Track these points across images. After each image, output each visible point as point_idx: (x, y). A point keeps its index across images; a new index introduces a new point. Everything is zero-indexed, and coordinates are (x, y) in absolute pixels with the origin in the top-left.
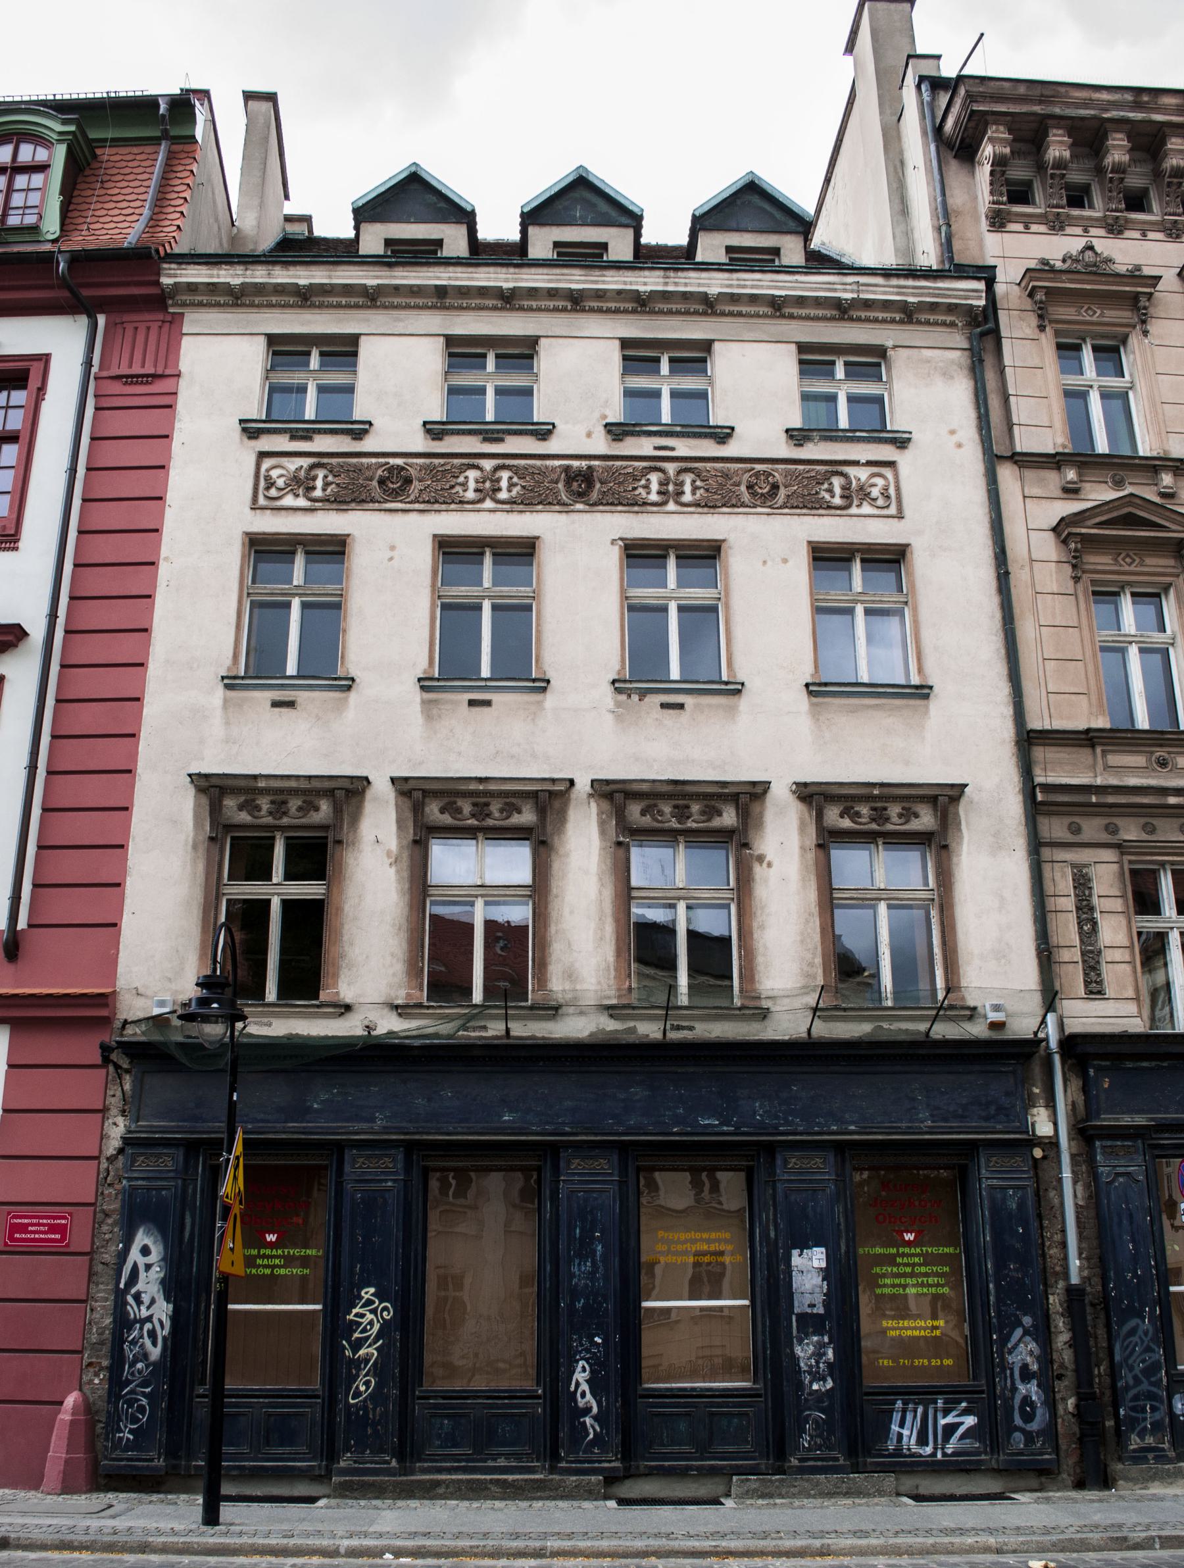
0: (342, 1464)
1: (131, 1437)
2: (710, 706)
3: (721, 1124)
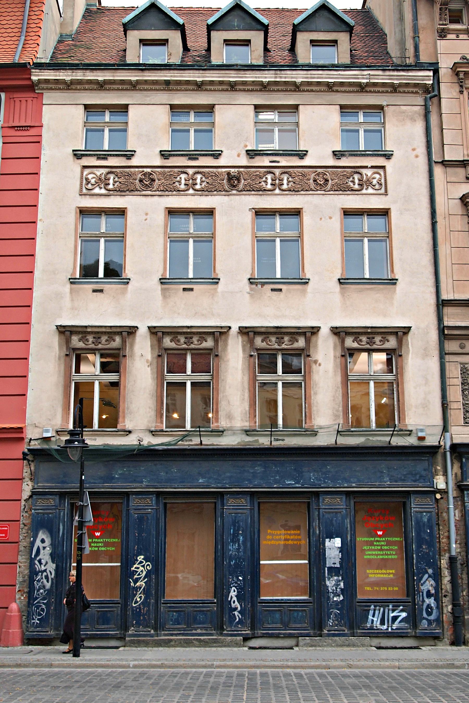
0: (130, 632)
1: (38, 622)
2: (294, 290)
3: (295, 483)
